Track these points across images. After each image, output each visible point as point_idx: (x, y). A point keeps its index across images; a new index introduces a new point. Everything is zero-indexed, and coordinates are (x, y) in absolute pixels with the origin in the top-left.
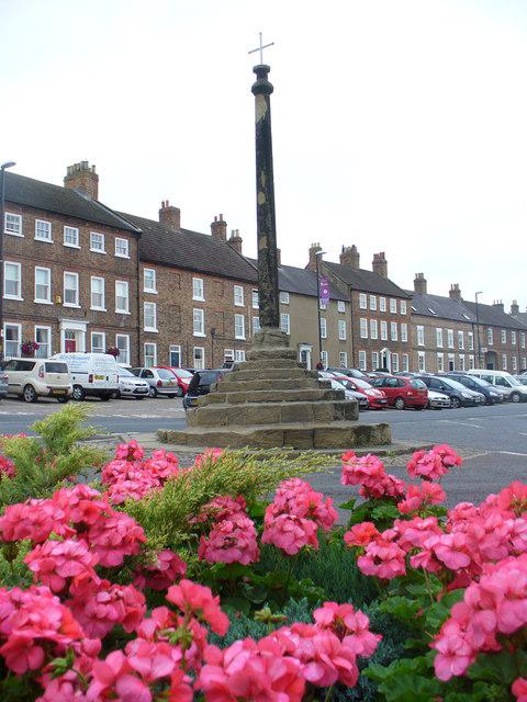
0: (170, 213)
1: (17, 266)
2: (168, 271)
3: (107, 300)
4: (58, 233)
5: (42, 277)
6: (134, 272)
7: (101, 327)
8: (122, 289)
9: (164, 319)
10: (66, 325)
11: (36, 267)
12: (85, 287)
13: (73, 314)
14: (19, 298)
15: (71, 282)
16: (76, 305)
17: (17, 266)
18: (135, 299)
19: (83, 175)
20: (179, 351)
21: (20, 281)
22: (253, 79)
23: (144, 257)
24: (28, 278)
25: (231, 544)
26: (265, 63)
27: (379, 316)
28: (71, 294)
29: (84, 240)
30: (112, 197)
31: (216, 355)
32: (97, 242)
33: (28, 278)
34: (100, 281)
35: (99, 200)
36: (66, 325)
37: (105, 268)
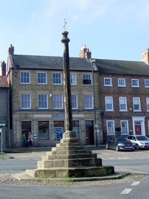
1: (138, 99)
4: (128, 82)
10: (135, 119)
11: (120, 97)
13: (138, 114)
14: (112, 110)
16: (140, 110)
17: (138, 99)
21: (126, 103)
22: (62, 37)
24: (116, 102)
26: (66, 31)
28: (137, 107)
33: (116, 102)
34: (125, 98)
36: (135, 119)
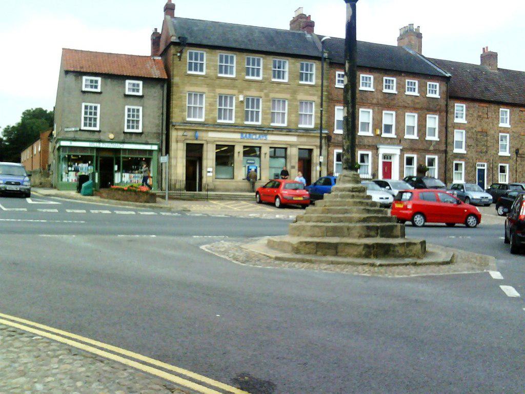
0: (489, 57)
2: (477, 105)
3: (419, 131)
4: (378, 83)
5: (411, 120)
6: (444, 108)
7: (413, 150)
8: (433, 122)
9: (471, 142)
10: (383, 150)
12: (400, 121)
13: (390, 142)
15: (389, 118)
16: (393, 135)
17: (392, 114)
18: (444, 129)
19: (412, 35)
20: (485, 168)
23: (452, 96)
24: (400, 121)
25: (29, 351)
27: (388, 102)
28: (388, 128)
29: (401, 87)
30: (431, 50)
31: (519, 170)
32: (412, 88)
35: (423, 54)
36: (383, 150)
37: (417, 106)
